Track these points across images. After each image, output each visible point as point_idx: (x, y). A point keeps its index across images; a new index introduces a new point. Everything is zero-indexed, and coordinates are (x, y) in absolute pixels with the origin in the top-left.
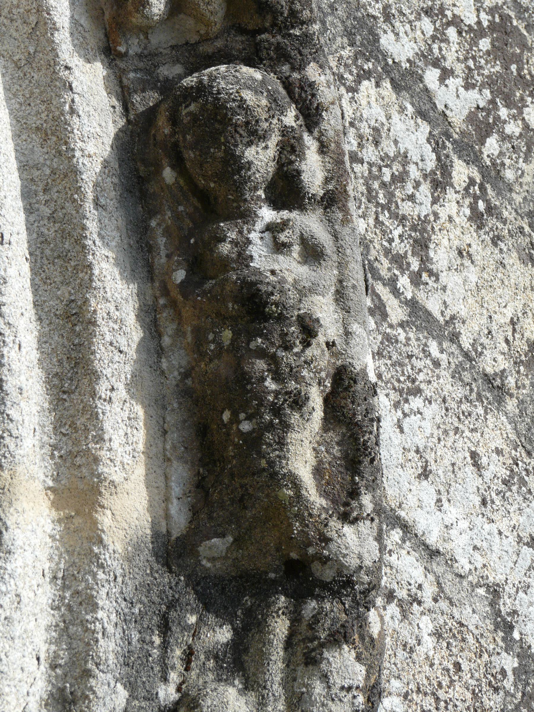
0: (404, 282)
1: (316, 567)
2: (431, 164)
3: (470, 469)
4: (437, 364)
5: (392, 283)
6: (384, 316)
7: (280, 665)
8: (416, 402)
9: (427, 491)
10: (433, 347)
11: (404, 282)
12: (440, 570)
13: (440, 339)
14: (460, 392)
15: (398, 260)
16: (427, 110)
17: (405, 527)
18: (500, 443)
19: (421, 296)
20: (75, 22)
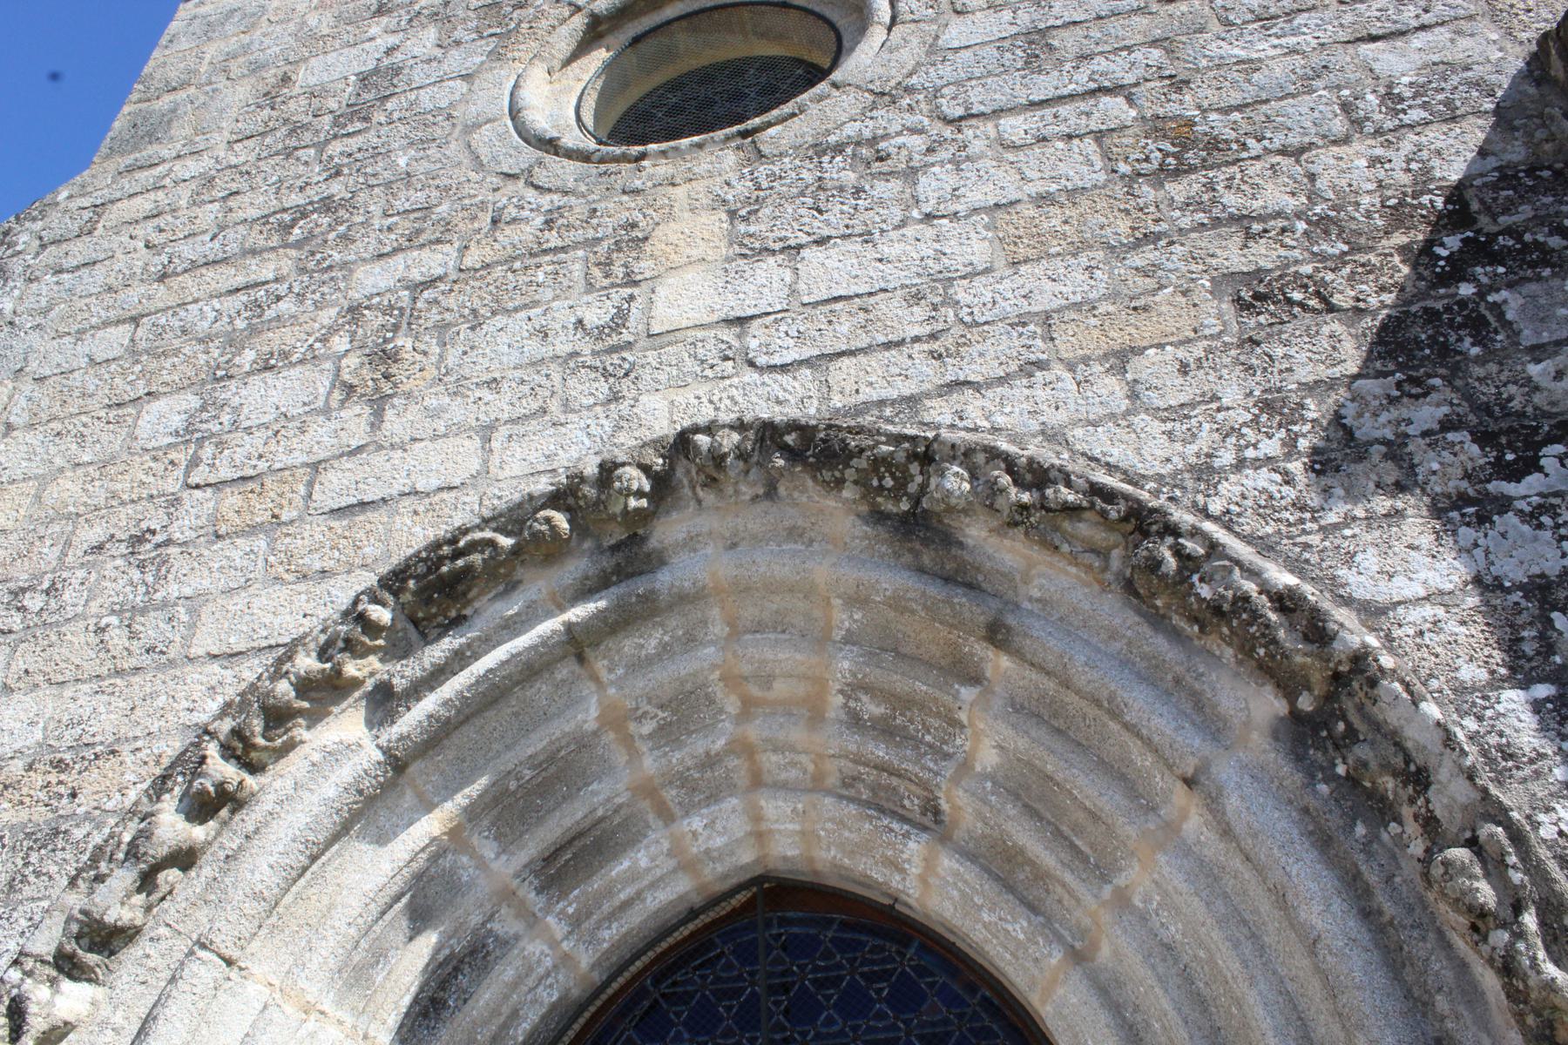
0: (1308, 526)
1: (1341, 668)
2: (1278, 478)
3: (1413, 553)
4: (1354, 536)
5: (1304, 532)
6: (1310, 546)
7: (729, 909)
8: (1358, 558)
9: (1399, 581)
10: (1348, 532)
11: (1308, 526)
12: (1439, 600)
13: (1347, 526)
14: (1377, 533)
15: (1302, 521)
16: (1257, 464)
17: (1399, 603)
18: (1418, 530)
19: (1323, 523)
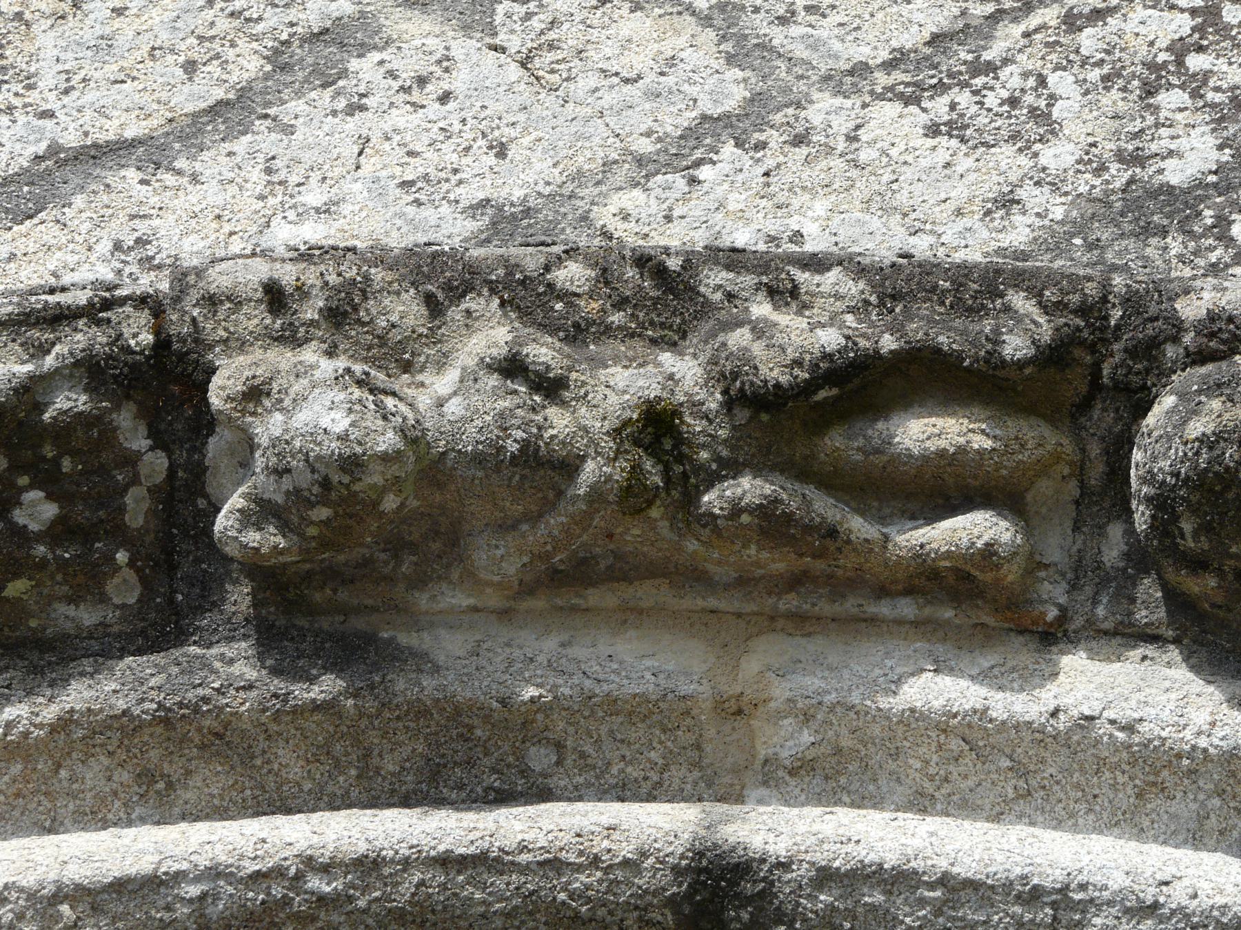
20: (982, 677)
